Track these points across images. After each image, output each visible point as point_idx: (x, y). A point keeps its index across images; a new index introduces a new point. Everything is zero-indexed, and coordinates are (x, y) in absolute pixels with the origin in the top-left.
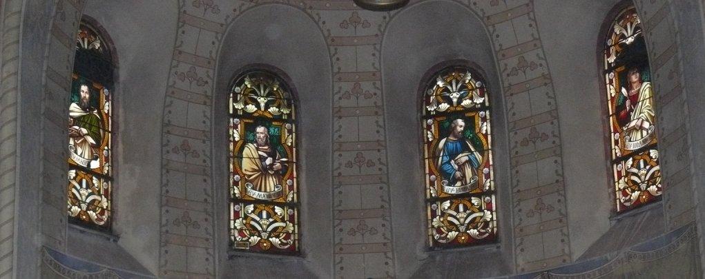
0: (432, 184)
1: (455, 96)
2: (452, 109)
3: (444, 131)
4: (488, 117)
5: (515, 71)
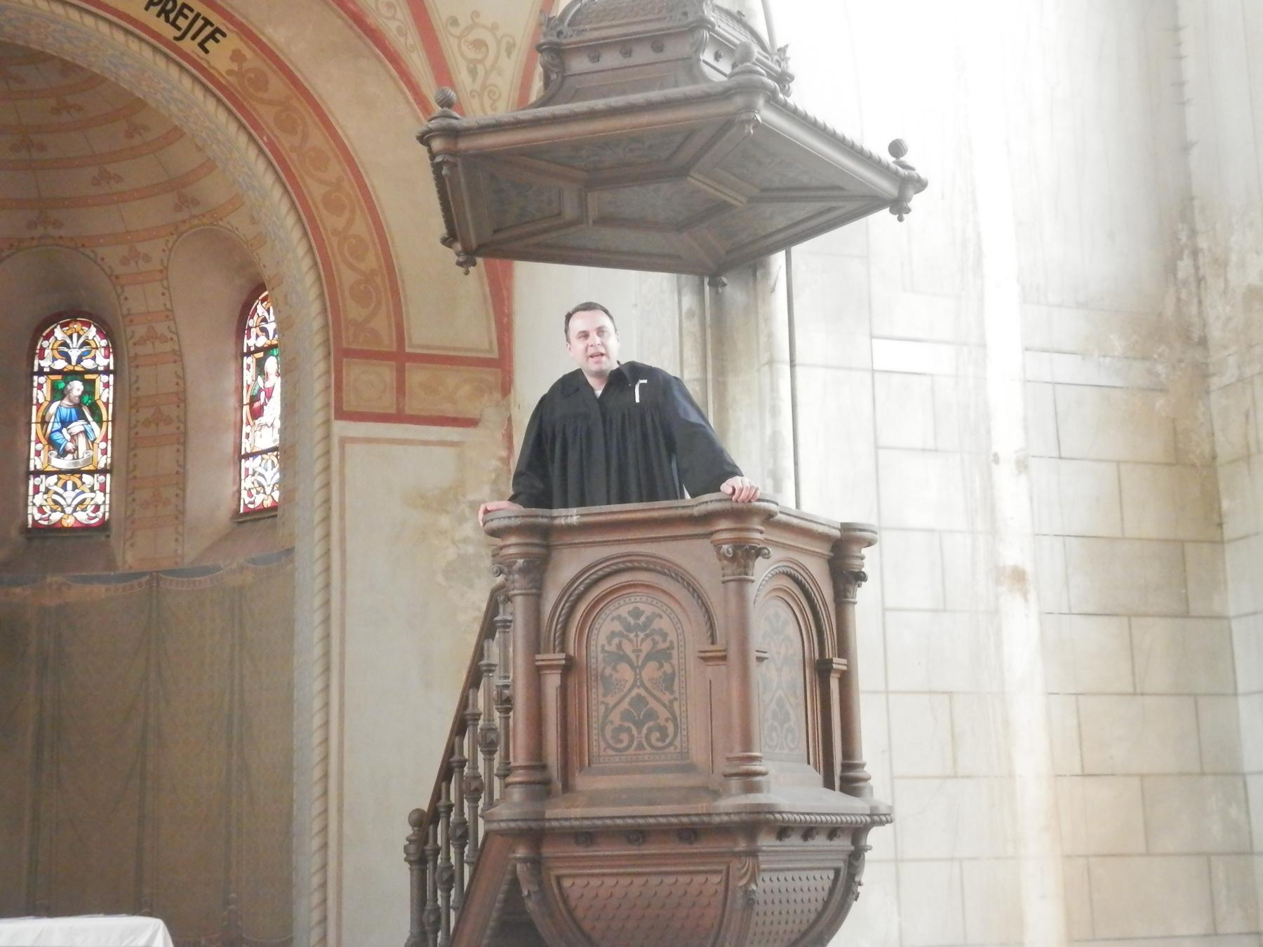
0: (38, 453)
1: (74, 354)
2: (71, 368)
3: (58, 393)
4: (111, 383)
5: (143, 341)
